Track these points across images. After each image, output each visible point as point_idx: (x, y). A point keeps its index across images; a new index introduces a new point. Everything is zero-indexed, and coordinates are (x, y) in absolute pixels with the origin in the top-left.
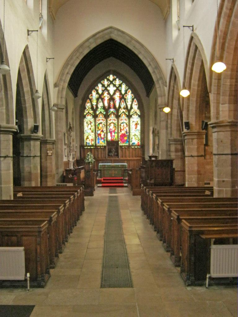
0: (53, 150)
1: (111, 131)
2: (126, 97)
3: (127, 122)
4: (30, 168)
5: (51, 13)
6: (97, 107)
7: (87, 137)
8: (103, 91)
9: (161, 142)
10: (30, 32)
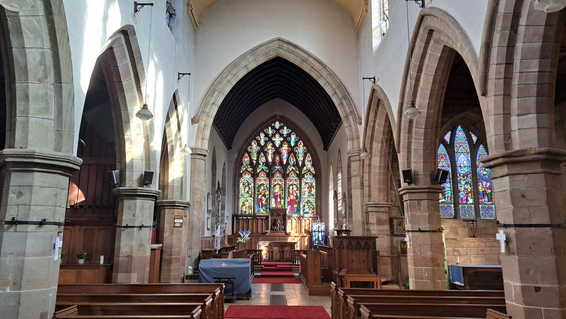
4: (132, 247)
6: (258, 164)
7: (244, 203)
8: (266, 142)
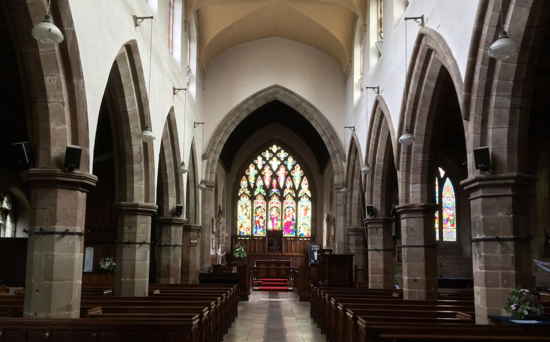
0: (198, 239)
1: (273, 218)
2: (293, 174)
3: (294, 206)
4: (169, 259)
5: (201, 66)
6: (255, 187)
8: (264, 166)
9: (337, 232)
10: (177, 91)
